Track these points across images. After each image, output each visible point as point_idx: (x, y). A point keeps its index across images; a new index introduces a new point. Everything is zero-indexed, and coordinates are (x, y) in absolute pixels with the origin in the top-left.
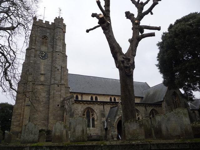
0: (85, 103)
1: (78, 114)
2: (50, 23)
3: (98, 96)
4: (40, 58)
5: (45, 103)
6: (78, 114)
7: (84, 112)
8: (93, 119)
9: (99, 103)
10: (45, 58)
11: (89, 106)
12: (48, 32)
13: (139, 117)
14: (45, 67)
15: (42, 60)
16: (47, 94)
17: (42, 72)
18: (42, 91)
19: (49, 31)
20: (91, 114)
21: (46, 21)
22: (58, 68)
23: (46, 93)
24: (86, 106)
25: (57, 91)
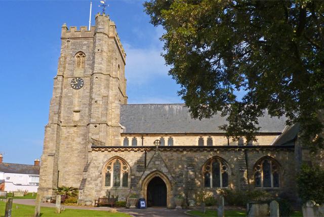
0: (110, 150)
1: (98, 167)
4: (73, 87)
5: (80, 152)
6: (98, 167)
7: (111, 164)
8: (225, 175)
9: (175, 149)
10: (76, 87)
11: (119, 154)
12: (85, 44)
13: (225, 173)
14: (80, 100)
15: (75, 91)
16: (83, 140)
17: (77, 109)
18: (76, 135)
19: (86, 42)
20: (122, 166)
23: (81, 138)
24: (113, 154)
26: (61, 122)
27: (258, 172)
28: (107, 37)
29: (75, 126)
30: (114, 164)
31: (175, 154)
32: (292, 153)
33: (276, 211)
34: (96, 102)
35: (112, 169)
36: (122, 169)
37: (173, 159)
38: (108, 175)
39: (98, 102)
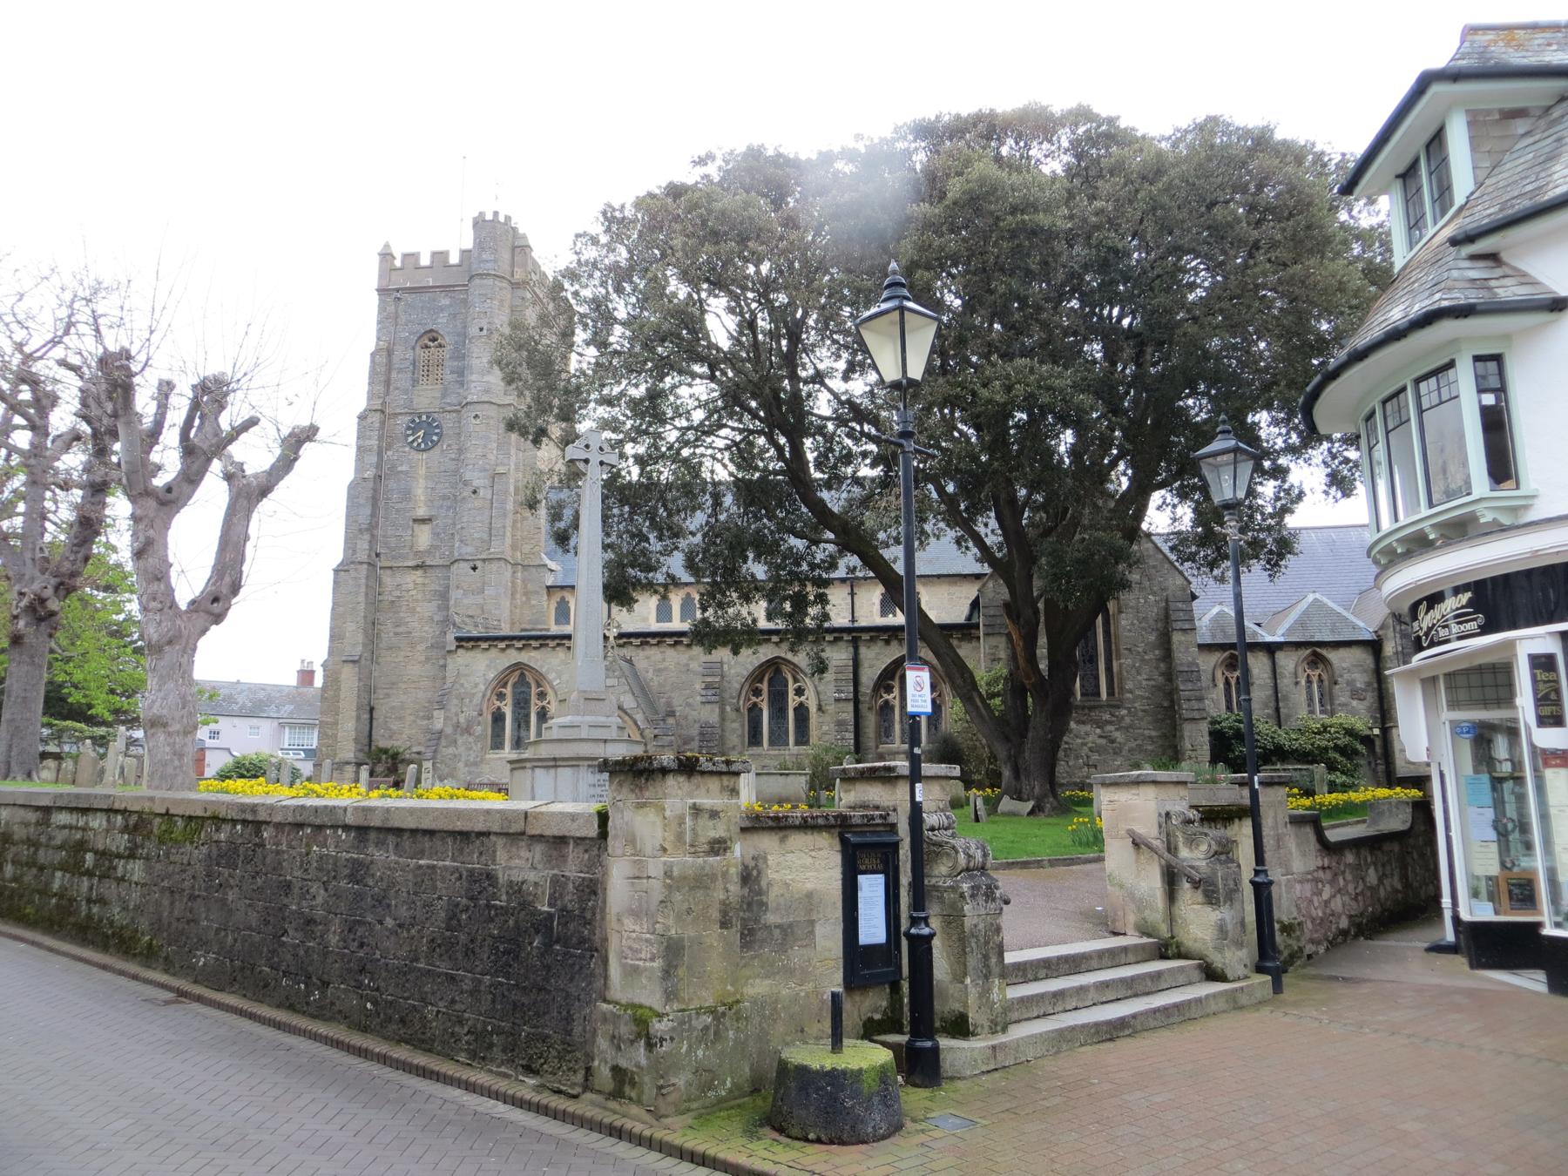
0: (502, 645)
2: (454, 259)
3: (924, 584)
7: (505, 686)
13: (801, 704)
17: (421, 512)
20: (534, 691)
21: (434, 254)
22: (476, 483)
23: (435, 603)
24: (513, 656)
25: (466, 593)
26: (377, 555)
27: (887, 702)
28: (505, 284)
29: (417, 567)
30: (515, 685)
31: (670, 652)
32: (974, 643)
33: (1491, 980)
34: (475, 492)
35: (509, 700)
36: (534, 699)
37: (666, 669)
38: (498, 718)
39: (481, 492)
